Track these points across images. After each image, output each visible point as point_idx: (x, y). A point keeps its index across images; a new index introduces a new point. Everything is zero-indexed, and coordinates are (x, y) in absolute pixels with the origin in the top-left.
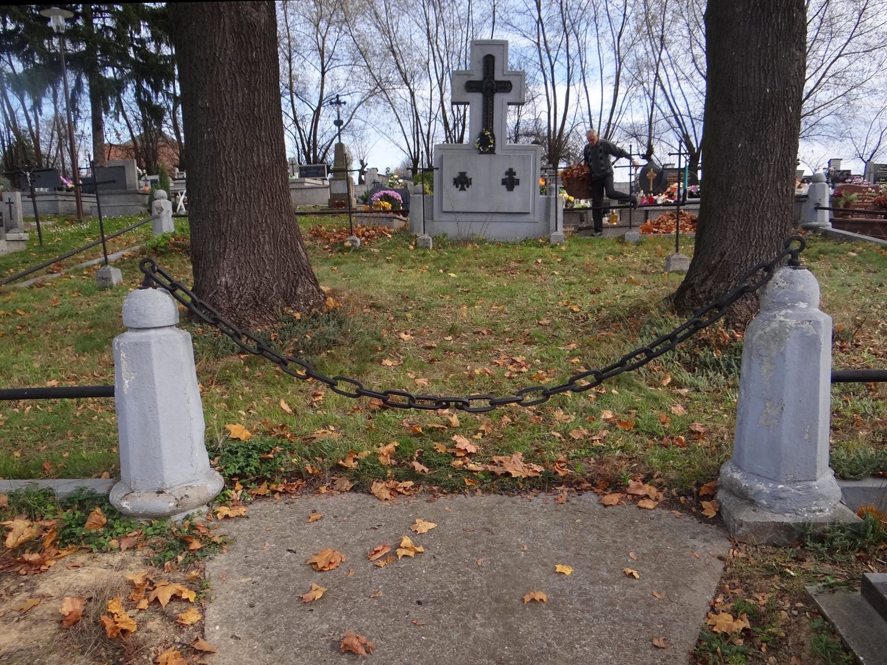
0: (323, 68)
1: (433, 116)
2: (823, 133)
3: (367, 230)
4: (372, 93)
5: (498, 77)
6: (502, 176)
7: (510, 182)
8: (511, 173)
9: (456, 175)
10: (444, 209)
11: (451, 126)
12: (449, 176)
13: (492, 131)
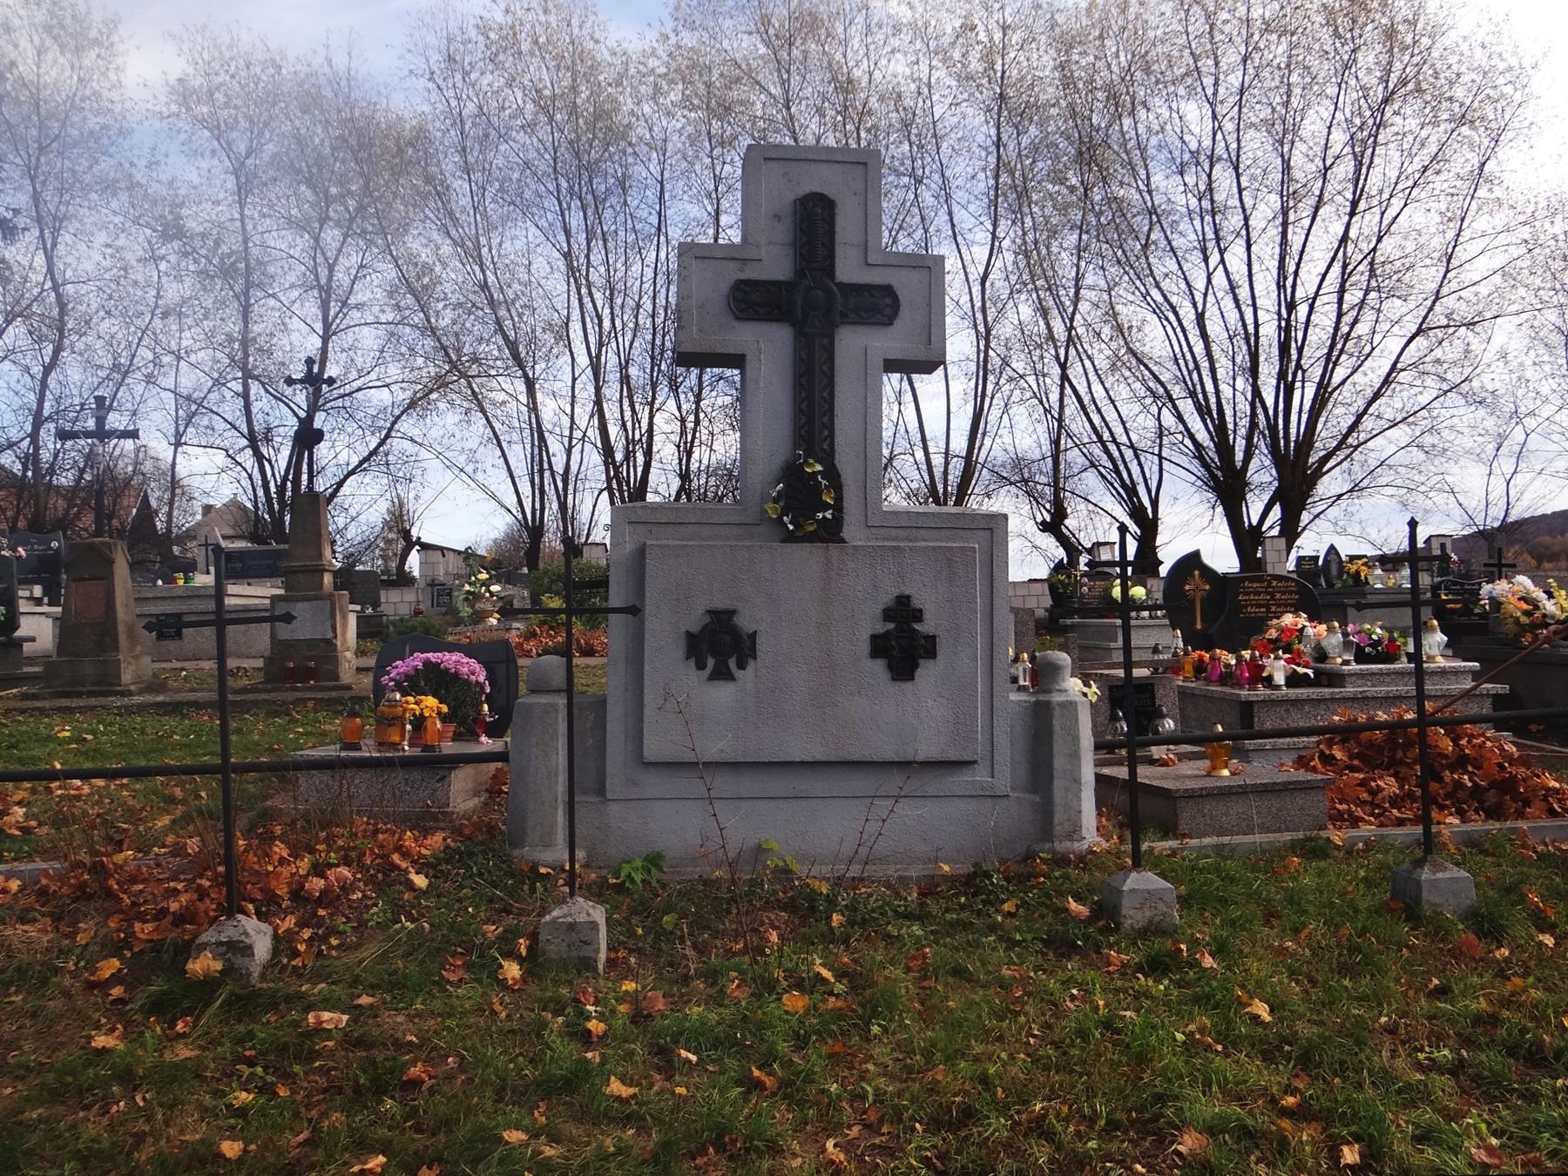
0: (327, 325)
1: (577, 434)
2: (1399, 482)
3: (319, 870)
4: (440, 383)
5: (848, 269)
6: (870, 623)
7: (903, 645)
8: (903, 612)
9: (694, 620)
10: (652, 751)
11: (619, 456)
12: (665, 628)
13: (828, 459)
